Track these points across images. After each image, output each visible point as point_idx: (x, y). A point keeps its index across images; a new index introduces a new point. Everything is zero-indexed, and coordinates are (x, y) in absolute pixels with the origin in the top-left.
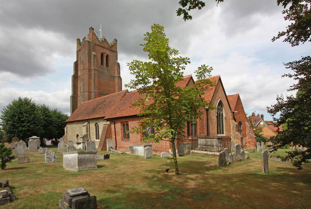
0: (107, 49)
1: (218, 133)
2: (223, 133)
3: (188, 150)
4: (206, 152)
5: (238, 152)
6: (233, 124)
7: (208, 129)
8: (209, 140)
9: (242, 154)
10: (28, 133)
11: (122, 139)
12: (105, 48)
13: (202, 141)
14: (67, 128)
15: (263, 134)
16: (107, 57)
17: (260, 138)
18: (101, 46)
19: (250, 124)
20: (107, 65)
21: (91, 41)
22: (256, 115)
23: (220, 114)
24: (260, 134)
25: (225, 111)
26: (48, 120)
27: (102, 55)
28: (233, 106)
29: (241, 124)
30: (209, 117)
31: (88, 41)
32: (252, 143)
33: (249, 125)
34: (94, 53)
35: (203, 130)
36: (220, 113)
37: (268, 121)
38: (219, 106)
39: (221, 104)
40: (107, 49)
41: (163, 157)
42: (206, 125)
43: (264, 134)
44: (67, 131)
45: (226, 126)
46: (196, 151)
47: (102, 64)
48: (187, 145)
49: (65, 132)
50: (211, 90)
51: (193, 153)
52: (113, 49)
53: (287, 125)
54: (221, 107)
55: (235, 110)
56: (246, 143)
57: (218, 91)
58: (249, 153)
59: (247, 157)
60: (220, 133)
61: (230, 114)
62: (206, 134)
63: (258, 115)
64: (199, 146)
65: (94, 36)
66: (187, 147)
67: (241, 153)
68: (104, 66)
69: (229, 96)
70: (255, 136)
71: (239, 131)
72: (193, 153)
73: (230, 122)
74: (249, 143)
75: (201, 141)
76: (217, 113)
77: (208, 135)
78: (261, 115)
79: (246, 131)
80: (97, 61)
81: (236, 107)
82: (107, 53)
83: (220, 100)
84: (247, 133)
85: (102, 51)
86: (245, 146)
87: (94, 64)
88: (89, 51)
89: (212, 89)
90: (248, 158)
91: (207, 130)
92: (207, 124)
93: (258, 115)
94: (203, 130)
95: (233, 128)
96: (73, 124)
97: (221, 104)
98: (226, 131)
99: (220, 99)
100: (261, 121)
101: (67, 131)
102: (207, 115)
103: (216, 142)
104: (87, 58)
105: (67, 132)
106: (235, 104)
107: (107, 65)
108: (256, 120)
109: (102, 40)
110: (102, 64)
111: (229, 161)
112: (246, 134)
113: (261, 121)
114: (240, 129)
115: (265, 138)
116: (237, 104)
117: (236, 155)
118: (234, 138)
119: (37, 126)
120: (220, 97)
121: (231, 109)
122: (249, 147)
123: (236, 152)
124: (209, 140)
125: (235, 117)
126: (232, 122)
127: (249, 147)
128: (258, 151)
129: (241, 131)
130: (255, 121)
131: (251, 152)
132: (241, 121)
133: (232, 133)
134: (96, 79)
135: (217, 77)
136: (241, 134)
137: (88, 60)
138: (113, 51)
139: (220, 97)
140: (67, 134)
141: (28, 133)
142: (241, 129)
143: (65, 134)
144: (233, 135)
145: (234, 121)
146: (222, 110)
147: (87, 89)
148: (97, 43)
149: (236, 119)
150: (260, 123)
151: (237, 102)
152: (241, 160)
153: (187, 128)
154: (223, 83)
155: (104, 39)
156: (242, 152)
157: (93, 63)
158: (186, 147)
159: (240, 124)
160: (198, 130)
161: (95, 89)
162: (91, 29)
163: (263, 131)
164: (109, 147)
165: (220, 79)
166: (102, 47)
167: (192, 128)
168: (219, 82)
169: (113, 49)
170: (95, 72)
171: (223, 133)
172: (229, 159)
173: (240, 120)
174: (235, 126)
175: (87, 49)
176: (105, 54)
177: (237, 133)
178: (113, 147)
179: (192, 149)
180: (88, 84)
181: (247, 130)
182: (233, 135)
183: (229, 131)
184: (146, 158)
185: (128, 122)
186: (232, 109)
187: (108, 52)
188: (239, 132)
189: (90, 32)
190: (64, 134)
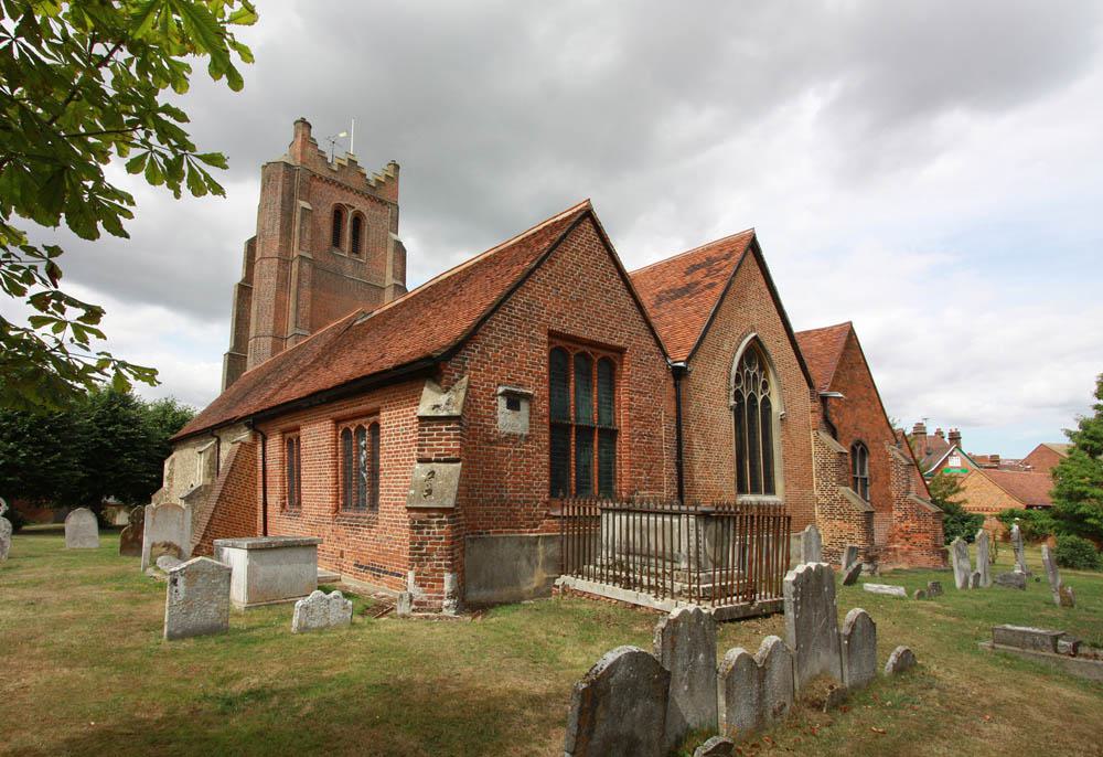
0: (357, 192)
1: (741, 489)
2: (770, 490)
3: (545, 576)
4: (629, 596)
5: (816, 630)
6: (822, 448)
7: (679, 466)
8: (652, 525)
9: (849, 637)
10: (9, 479)
11: (283, 505)
12: (351, 190)
13: (638, 523)
14: (173, 460)
15: (965, 501)
16: (358, 220)
17: (952, 514)
18: (334, 182)
19: (909, 456)
20: (356, 248)
21: (299, 163)
22: (931, 432)
23: (756, 400)
24: (951, 499)
25: (782, 389)
26: (121, 435)
27: (338, 213)
28: (823, 373)
29: (864, 452)
30: (692, 409)
31: (286, 165)
32: (921, 539)
33: (904, 457)
34: (304, 204)
35: (649, 470)
36: (752, 399)
37: (978, 455)
38: (750, 365)
39: (756, 354)
40: (357, 192)
41: (303, 629)
42: (672, 446)
43: (970, 500)
44: (172, 472)
45: (785, 459)
46: (581, 584)
47: (337, 240)
48: (541, 548)
49: (165, 479)
50: (708, 291)
51: (564, 593)
52: (383, 194)
53: (178, 714)
54: (762, 368)
55: (834, 387)
56: (891, 538)
57: (742, 298)
58: (910, 593)
59: (892, 659)
60: (756, 490)
61: (804, 403)
62: (668, 490)
63: (939, 433)
64: (604, 556)
65: (309, 149)
66: (541, 558)
67: (845, 630)
68: (343, 251)
69: (807, 333)
70: (934, 509)
71: (860, 484)
72: (565, 590)
73: (809, 442)
74: (907, 539)
75: (614, 527)
76: (738, 396)
77: (680, 495)
78: (951, 434)
79: (888, 483)
80: (316, 232)
81: (837, 376)
82: (358, 206)
83: (755, 337)
84: (894, 494)
85: (338, 198)
86: (888, 550)
87: (301, 242)
88: (287, 198)
89: (712, 285)
90: (906, 664)
91: (674, 471)
92: (679, 440)
93: (939, 433)
94: (649, 470)
95: (824, 467)
96: (187, 447)
97: (756, 354)
98: (786, 479)
99: (754, 334)
100: (951, 454)
101: (172, 472)
102: (678, 399)
103: (693, 538)
104: (278, 221)
105: (170, 479)
106: (835, 363)
107: (356, 248)
108: (928, 449)
109: (342, 162)
110: (337, 240)
111: (714, 732)
112: (889, 496)
113: (951, 454)
114: (862, 472)
115: (973, 516)
116: (840, 366)
117: (798, 661)
118: (830, 514)
119: (46, 453)
120: (751, 321)
121: (810, 384)
122: (905, 554)
123: (791, 634)
124: (652, 525)
125: (835, 421)
126: (816, 438)
127: (905, 554)
128: (959, 584)
129: (865, 485)
130: (928, 454)
131: (921, 595)
132: (864, 439)
133: (816, 493)
134: (306, 292)
135: (739, 238)
136: (864, 496)
137: (281, 228)
138: (381, 201)
139: (751, 321)
140: (172, 486)
141: (9, 479)
142: (867, 474)
143: (165, 484)
144: (822, 500)
145: (826, 437)
146: (765, 385)
147: (271, 325)
148: (321, 170)
149: (840, 430)
150: (946, 460)
151: (843, 355)
152: (842, 701)
153: (551, 459)
154: (771, 272)
155: (349, 159)
156: (853, 626)
157: (297, 239)
158: (536, 554)
159: (860, 450)
160: (623, 471)
161: (299, 324)
162: (301, 124)
163: (964, 489)
164: (153, 545)
165: (753, 247)
166: (340, 185)
167: (583, 460)
168: (750, 257)
169: (384, 194)
170: (300, 265)
171: (770, 490)
172: (722, 701)
173: (857, 436)
174: (832, 459)
175: (280, 190)
176: (351, 212)
177: (846, 491)
178: (177, 542)
179: (563, 570)
180: (273, 310)
181: (893, 479)
182: (822, 500)
183: (801, 480)
184: (172, 637)
185: (297, 429)
186: (818, 383)
187: (361, 205)
188: (855, 489)
189: (296, 136)
190: (161, 485)
